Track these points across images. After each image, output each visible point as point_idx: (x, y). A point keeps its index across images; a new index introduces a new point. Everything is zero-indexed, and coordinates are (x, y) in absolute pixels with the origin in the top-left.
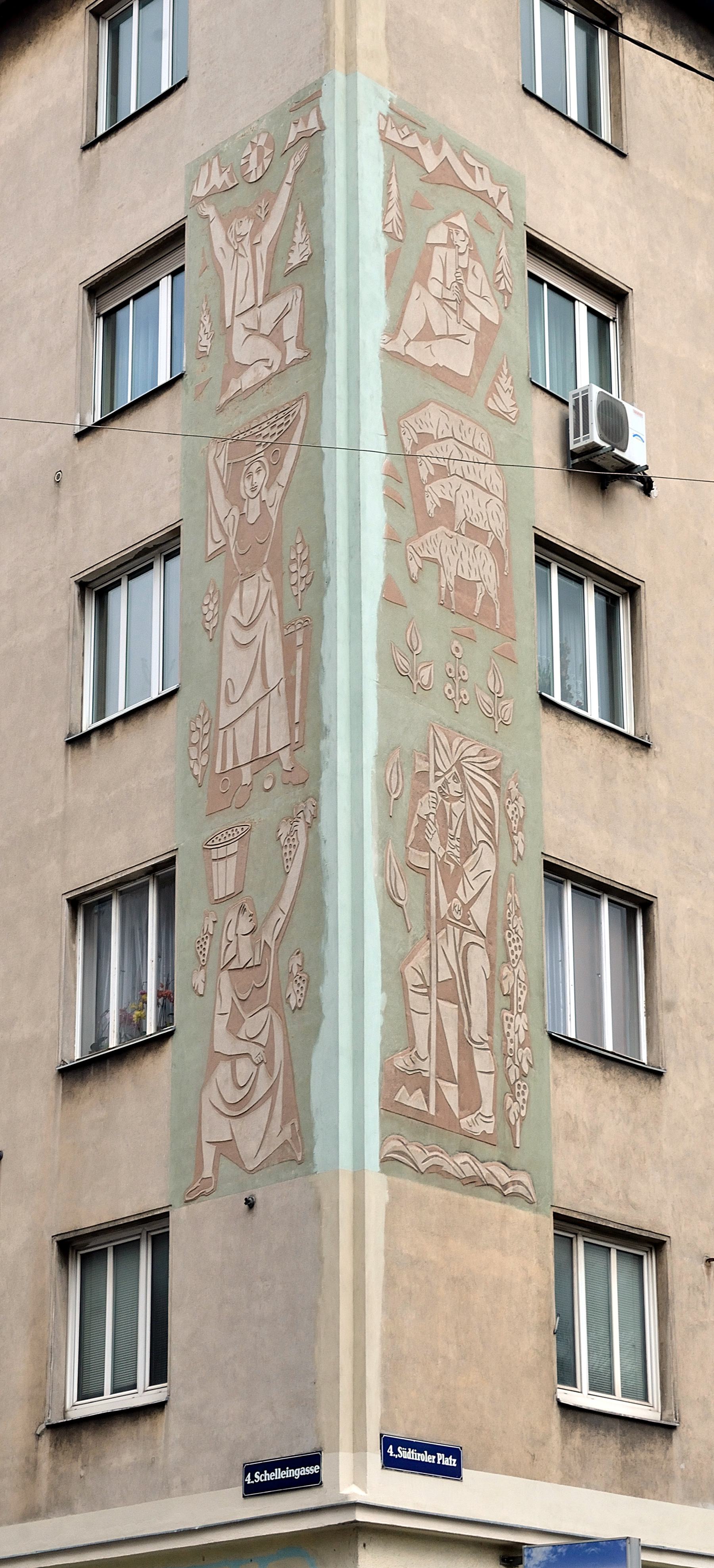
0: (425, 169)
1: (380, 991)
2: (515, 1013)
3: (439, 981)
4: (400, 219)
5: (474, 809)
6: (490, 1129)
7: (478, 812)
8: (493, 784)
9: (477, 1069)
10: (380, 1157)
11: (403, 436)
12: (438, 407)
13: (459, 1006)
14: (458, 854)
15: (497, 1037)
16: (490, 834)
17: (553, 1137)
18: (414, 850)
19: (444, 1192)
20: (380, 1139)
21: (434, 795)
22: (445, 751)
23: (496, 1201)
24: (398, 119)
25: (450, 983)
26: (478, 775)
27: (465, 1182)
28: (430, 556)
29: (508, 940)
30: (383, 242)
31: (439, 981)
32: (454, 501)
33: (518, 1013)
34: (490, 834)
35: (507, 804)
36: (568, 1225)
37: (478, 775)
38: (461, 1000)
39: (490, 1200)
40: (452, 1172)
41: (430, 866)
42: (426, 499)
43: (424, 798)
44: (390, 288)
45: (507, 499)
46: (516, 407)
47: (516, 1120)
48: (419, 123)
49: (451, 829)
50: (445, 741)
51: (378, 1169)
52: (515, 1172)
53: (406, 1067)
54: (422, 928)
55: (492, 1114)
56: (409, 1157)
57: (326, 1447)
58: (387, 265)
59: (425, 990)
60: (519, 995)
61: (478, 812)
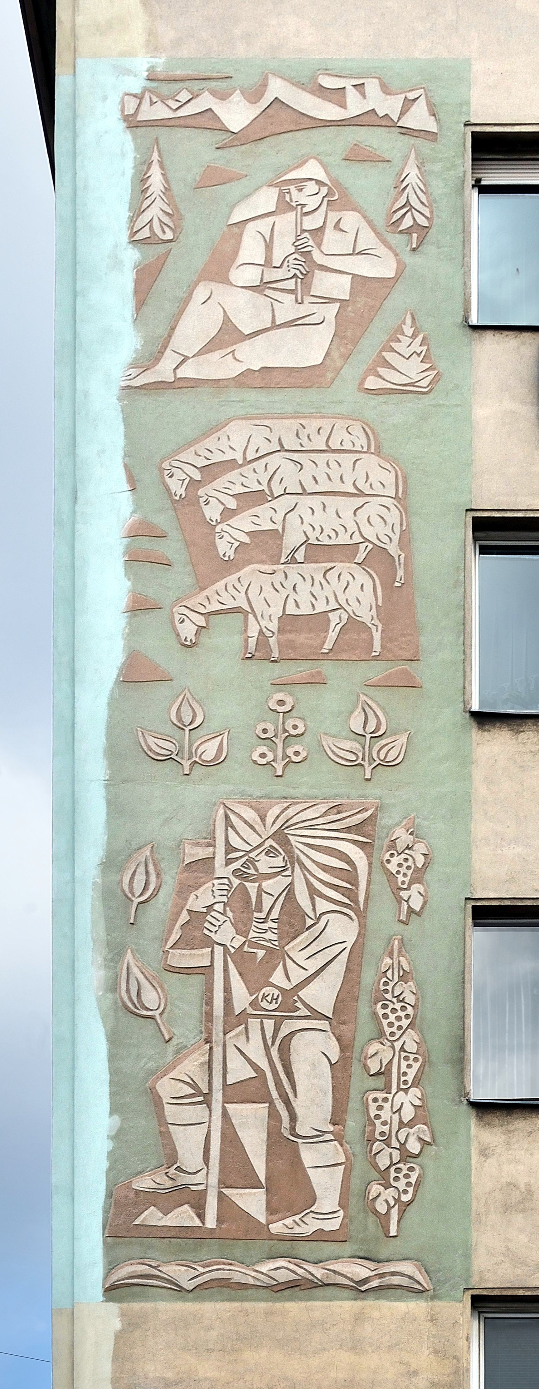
0: (228, 131)
1: (108, 1116)
2: (394, 1090)
3: (229, 1082)
4: (168, 214)
5: (312, 879)
6: (333, 1225)
7: (321, 881)
8: (355, 842)
9: (306, 1166)
10: (103, 1285)
11: (167, 478)
12: (249, 422)
13: (271, 1103)
14: (275, 937)
15: (353, 1124)
16: (347, 901)
17: (473, 1214)
18: (189, 902)
19: (236, 1304)
20: (104, 1267)
21: (226, 881)
22: (252, 827)
23: (346, 1299)
24: (165, 89)
25: (256, 1083)
26: (323, 838)
27: (276, 1289)
28: (224, 607)
29: (381, 1012)
30: (131, 256)
31: (229, 1082)
32: (281, 531)
33: (399, 1089)
34: (347, 901)
35: (387, 856)
36: (527, 1305)
37: (323, 838)
38: (275, 1094)
39: (330, 1300)
40: (251, 1281)
41: (212, 961)
42: (218, 541)
43: (201, 889)
44: (145, 309)
45: (404, 492)
46: (434, 369)
47: (390, 1208)
48: (215, 75)
49: (260, 911)
50: (250, 815)
51: (102, 1299)
52: (381, 1264)
53: (158, 1186)
54: (196, 1032)
55: (339, 1208)
56: (164, 1278)
57: (465, 501)
58: (103, 1227)
59: (201, 1099)
60: (404, 1068)
61: (321, 881)
